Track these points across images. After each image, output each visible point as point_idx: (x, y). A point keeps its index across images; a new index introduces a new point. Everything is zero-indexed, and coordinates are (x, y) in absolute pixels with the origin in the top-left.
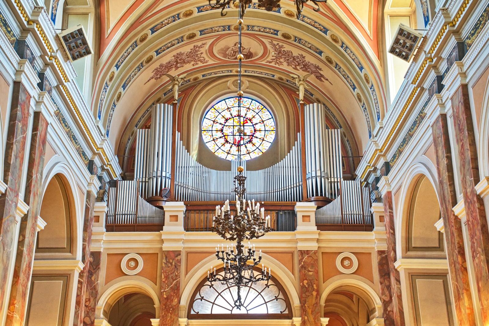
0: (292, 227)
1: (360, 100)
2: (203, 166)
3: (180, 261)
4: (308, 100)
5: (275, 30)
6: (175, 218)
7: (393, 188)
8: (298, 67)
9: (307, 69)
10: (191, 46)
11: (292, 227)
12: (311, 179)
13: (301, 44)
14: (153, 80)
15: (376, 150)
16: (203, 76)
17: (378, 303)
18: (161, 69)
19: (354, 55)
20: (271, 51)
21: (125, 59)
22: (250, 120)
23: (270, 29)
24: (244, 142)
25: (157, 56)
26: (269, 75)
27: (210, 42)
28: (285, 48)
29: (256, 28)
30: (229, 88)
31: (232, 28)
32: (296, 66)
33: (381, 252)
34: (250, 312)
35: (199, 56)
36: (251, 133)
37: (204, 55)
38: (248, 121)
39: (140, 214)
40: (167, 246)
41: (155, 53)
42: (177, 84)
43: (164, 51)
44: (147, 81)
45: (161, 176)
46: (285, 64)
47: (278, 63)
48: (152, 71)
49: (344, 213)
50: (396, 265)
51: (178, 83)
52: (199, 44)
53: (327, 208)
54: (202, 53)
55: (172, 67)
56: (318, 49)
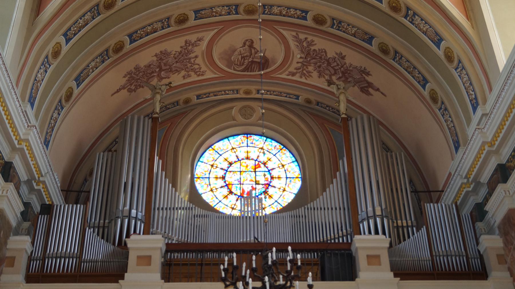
2: (197, 208)
5: (303, 11)
8: (334, 78)
9: (347, 79)
12: (367, 221)
13: (341, 30)
14: (124, 92)
16: (198, 97)
18: (137, 75)
19: (426, 23)
20: (295, 54)
21: (80, 31)
22: (265, 164)
23: (296, 9)
24: (256, 194)
25: (130, 44)
26: (291, 96)
27: (208, 36)
28: (316, 44)
29: (276, 10)
30: (234, 120)
31: (241, 9)
32: (330, 76)
35: (192, 60)
36: (267, 181)
38: (262, 166)
39: (86, 256)
41: (127, 37)
42: (158, 93)
43: (141, 38)
44: (116, 90)
45: (129, 217)
46: (315, 74)
47: (304, 75)
48: (123, 75)
49: (434, 254)
51: (160, 92)
52: (193, 38)
54: (196, 57)
55: (152, 75)
56: (366, 33)
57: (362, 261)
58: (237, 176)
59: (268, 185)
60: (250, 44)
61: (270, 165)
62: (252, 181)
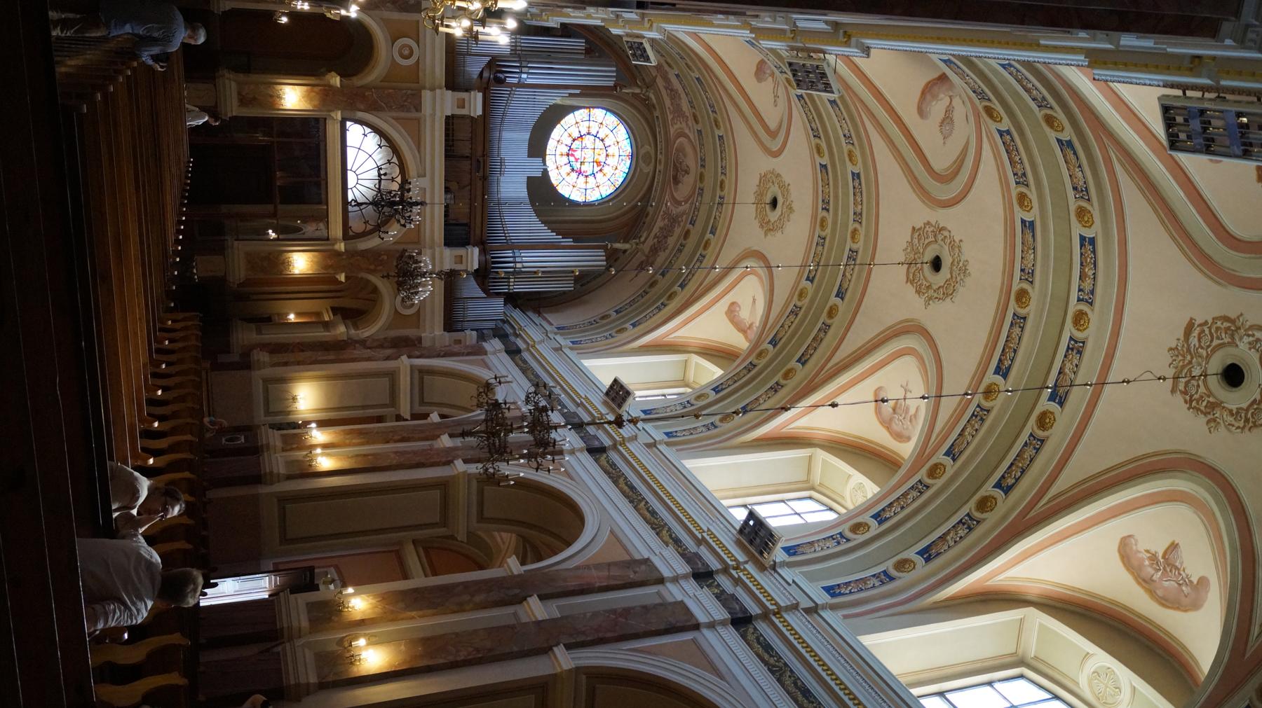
0: (450, 242)
1: (603, 318)
3: (408, 111)
4: (612, 256)
6: (461, 104)
7: (491, 359)
10: (688, 114)
11: (450, 242)
15: (534, 342)
17: (366, 333)
22: (601, 170)
27: (692, 137)
33: (420, 339)
34: (350, 191)
37: (678, 125)
38: (599, 168)
39: (468, 59)
40: (427, 95)
45: (521, 72)
50: (404, 358)
53: (473, 283)
57: (460, 251)
58: (590, 145)
59: (580, 173)
60: (687, 172)
61: (599, 175)
62: (585, 158)
